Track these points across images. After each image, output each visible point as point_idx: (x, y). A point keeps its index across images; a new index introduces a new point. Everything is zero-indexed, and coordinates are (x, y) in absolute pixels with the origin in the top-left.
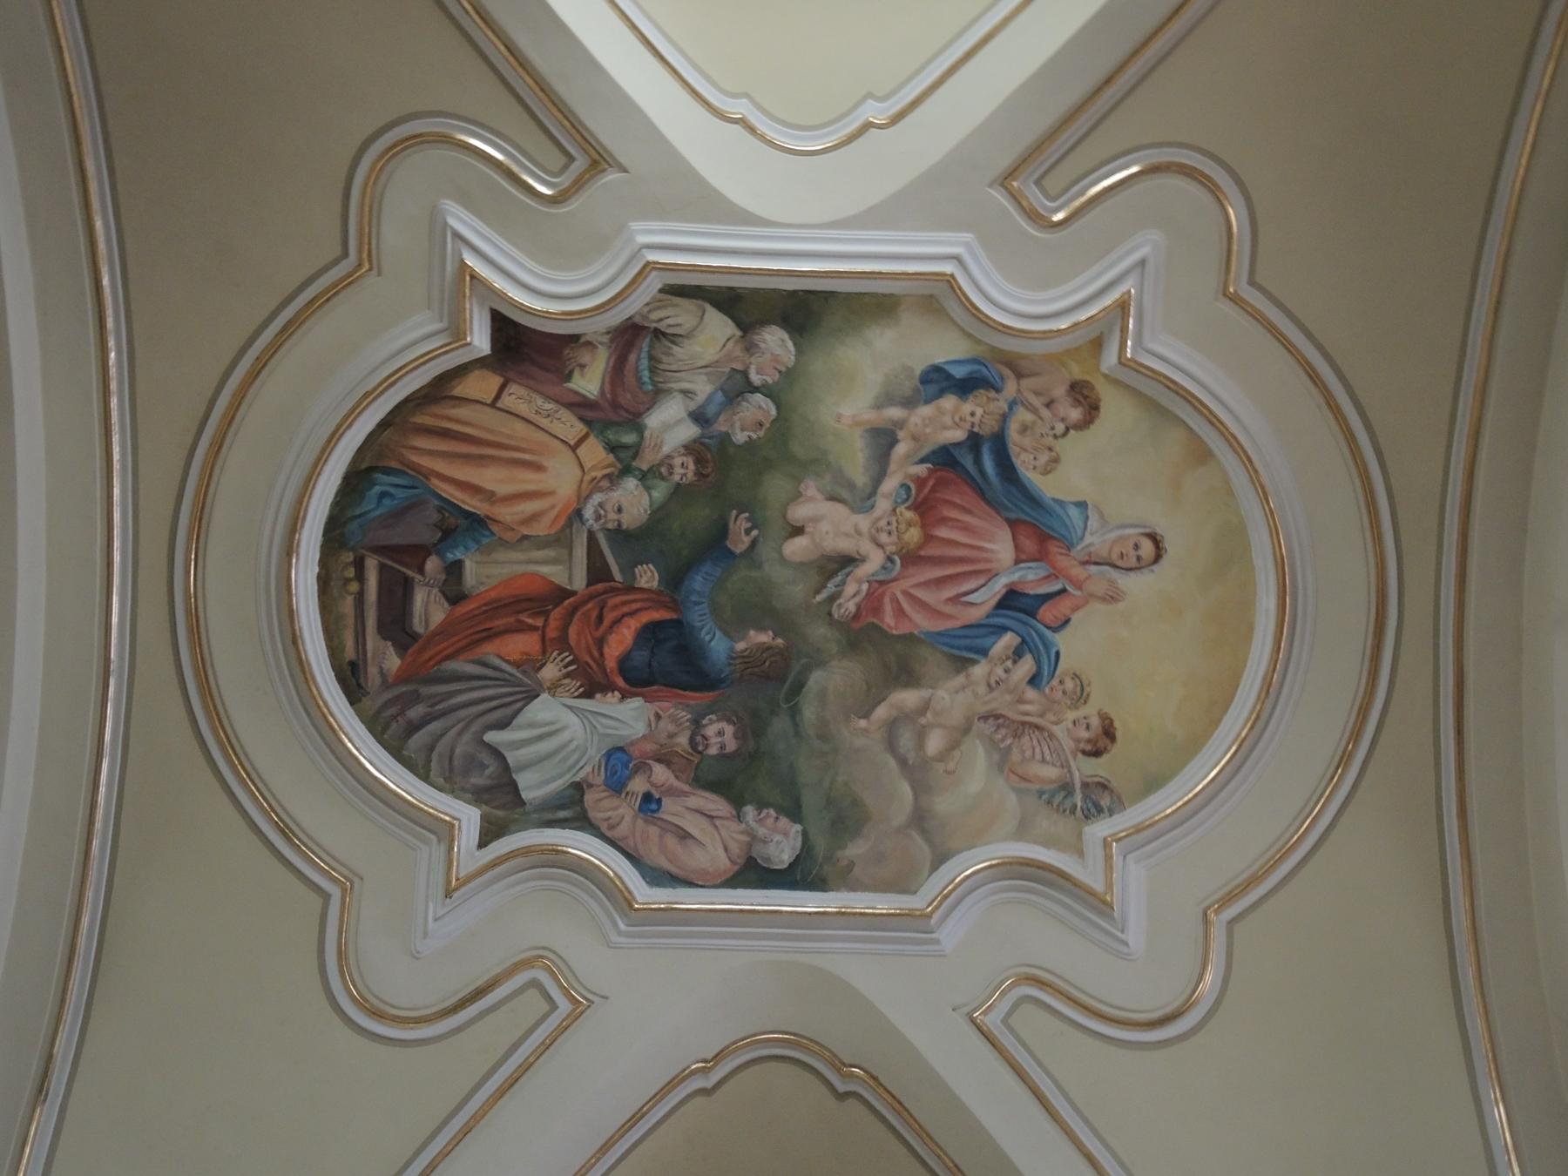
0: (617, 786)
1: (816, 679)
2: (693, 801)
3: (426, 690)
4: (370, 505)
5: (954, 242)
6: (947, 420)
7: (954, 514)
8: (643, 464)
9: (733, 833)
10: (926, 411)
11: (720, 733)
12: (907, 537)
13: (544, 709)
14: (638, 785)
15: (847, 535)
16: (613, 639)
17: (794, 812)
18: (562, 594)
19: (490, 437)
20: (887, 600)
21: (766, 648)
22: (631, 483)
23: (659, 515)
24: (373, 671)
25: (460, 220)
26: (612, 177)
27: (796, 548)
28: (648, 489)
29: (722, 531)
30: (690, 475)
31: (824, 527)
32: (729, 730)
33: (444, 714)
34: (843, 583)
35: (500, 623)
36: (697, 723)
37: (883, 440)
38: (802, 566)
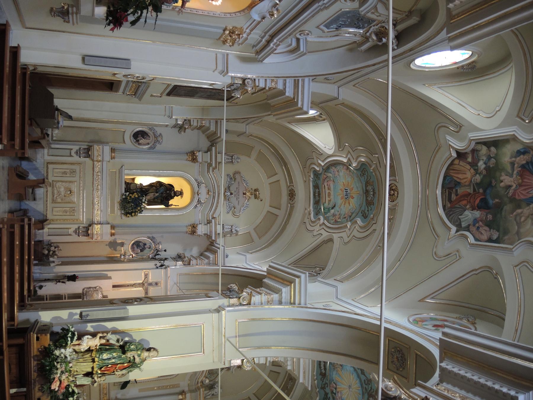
0: (474, 225)
1: (505, 207)
2: (484, 228)
3: (453, 209)
4: (446, 182)
5: (514, 128)
6: (522, 159)
7: (526, 177)
8: (479, 172)
9: (489, 234)
10: (518, 158)
11: (490, 217)
12: (519, 181)
13: (467, 213)
14: (477, 225)
15: (510, 182)
16: (476, 201)
17: (498, 231)
18: (470, 194)
19: (459, 170)
20: (517, 194)
21: (498, 202)
22: (478, 175)
23: (482, 180)
24: (447, 206)
25: (448, 137)
26: (463, 127)
27: (502, 184)
28: (480, 176)
29: (491, 182)
30: (485, 173)
31: (506, 181)
32: (491, 216)
33: (455, 213)
34: (510, 190)
35: (462, 199)
36: (487, 215)
37: (513, 164)
38: (503, 187)
